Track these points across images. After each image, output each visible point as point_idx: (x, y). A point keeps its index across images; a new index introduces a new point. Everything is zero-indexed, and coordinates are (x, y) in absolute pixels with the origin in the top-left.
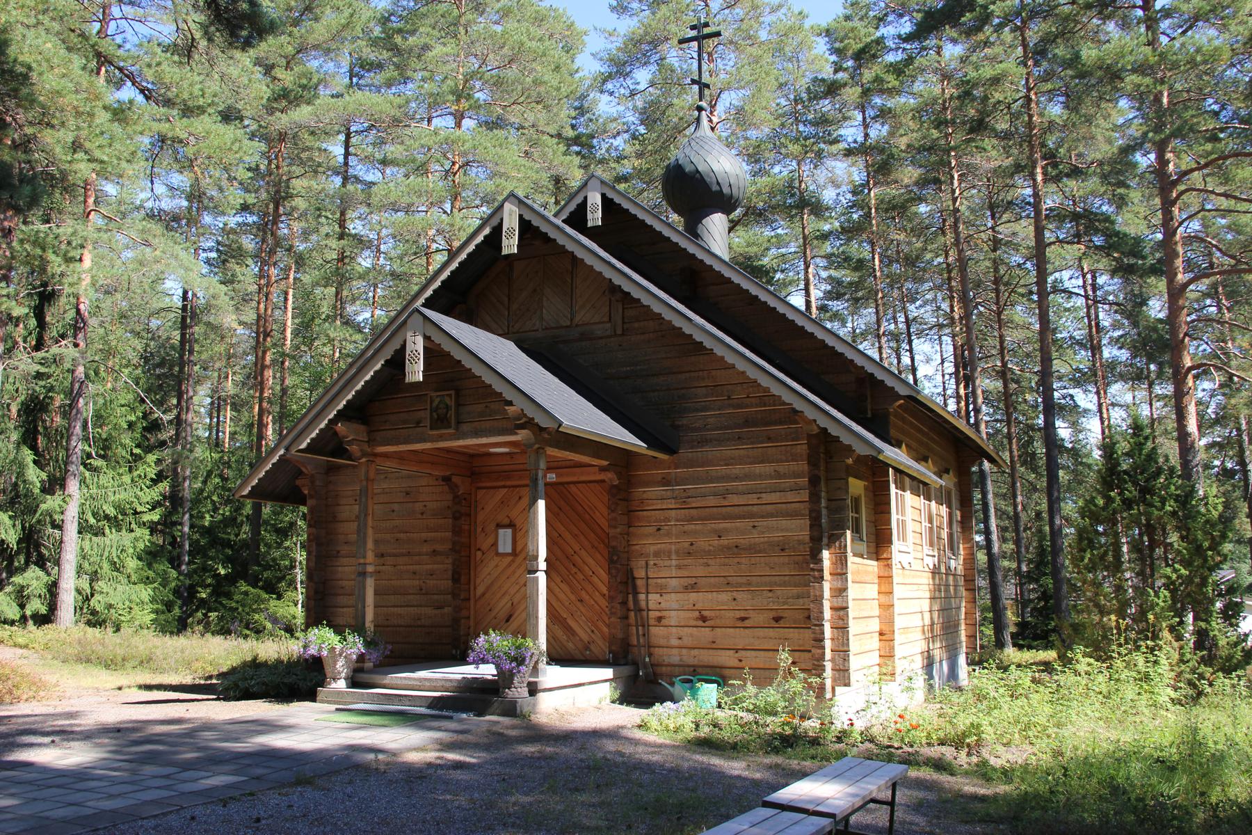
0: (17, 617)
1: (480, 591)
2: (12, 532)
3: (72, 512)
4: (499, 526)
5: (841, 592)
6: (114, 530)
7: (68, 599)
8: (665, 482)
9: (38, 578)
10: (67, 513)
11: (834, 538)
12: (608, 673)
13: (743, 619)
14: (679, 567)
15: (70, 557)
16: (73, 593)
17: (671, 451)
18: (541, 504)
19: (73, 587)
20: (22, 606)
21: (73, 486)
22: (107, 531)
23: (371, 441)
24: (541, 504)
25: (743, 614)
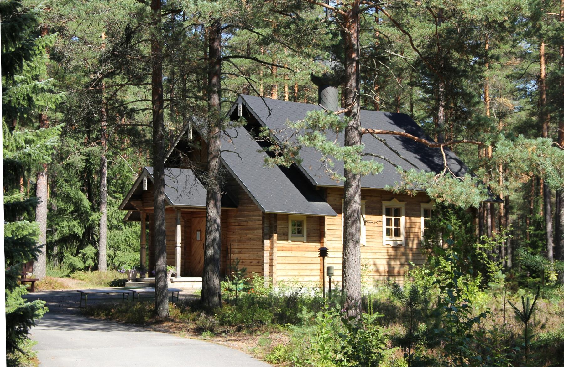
0: (83, 267)
1: (193, 253)
2: (80, 229)
3: (104, 220)
4: (198, 231)
5: (271, 254)
6: (127, 227)
7: (103, 259)
8: (235, 217)
9: (91, 250)
10: (101, 220)
11: (270, 238)
12: (200, 279)
13: (251, 262)
14: (238, 245)
15: (103, 242)
16: (106, 256)
17: (236, 207)
18: (179, 227)
19: (105, 254)
20: (85, 262)
21: (104, 208)
22: (123, 227)
23: (143, 206)
24: (179, 227)
25: (251, 261)
